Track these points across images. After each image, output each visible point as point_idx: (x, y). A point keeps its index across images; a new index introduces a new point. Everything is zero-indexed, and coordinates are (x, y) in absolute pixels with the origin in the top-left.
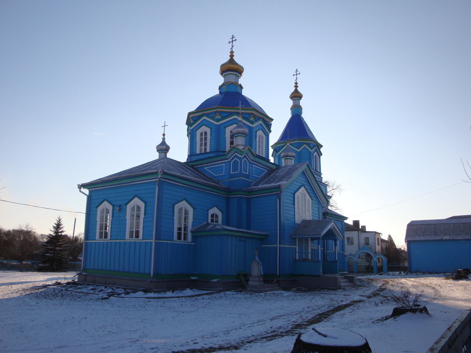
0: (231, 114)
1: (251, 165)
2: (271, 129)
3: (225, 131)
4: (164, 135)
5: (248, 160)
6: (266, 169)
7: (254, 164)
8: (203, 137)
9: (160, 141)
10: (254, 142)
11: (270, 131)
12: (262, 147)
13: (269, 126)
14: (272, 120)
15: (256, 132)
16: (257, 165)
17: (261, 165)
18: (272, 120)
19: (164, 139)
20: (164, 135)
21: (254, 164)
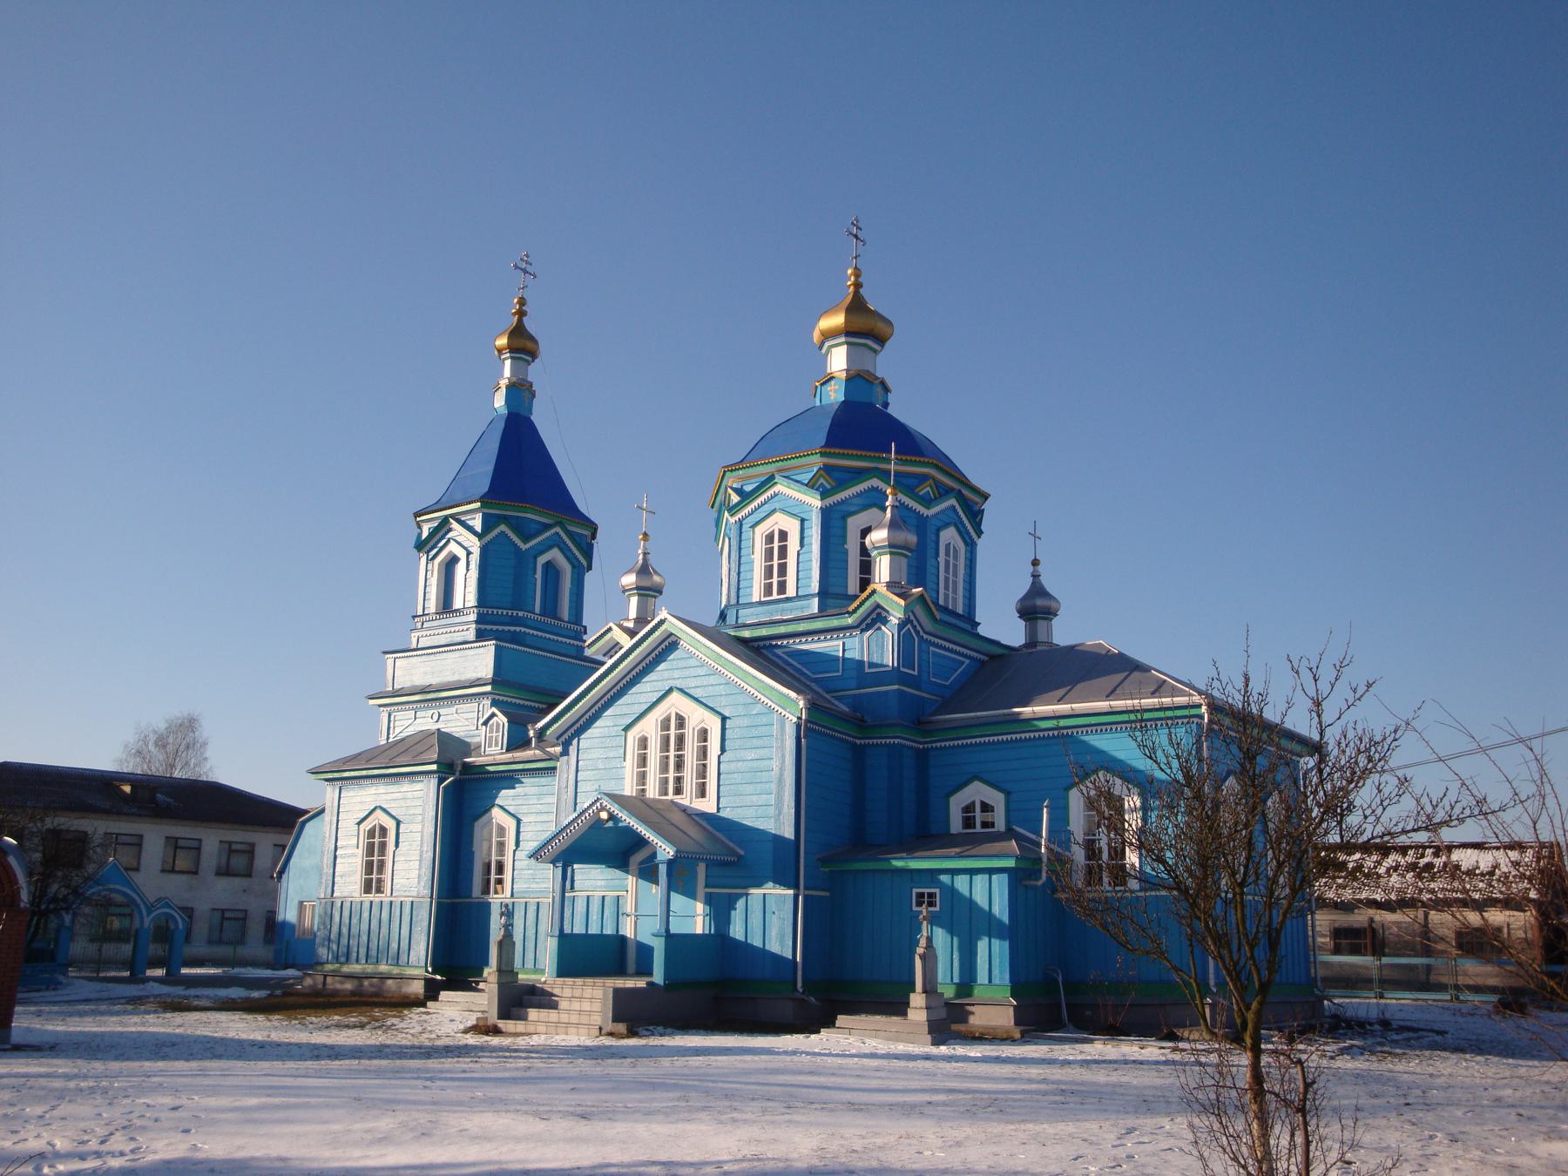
0: (859, 474)
1: (924, 646)
2: (983, 528)
3: (845, 528)
4: (1035, 563)
5: (917, 633)
6: (966, 656)
7: (934, 644)
8: (776, 545)
9: (1025, 585)
10: (931, 570)
11: (979, 533)
12: (955, 583)
13: (976, 516)
14: (986, 497)
15: (938, 530)
16: (940, 647)
17: (958, 648)
18: (986, 497)
19: (1035, 576)
20: (1035, 563)
21: (934, 644)
